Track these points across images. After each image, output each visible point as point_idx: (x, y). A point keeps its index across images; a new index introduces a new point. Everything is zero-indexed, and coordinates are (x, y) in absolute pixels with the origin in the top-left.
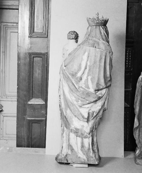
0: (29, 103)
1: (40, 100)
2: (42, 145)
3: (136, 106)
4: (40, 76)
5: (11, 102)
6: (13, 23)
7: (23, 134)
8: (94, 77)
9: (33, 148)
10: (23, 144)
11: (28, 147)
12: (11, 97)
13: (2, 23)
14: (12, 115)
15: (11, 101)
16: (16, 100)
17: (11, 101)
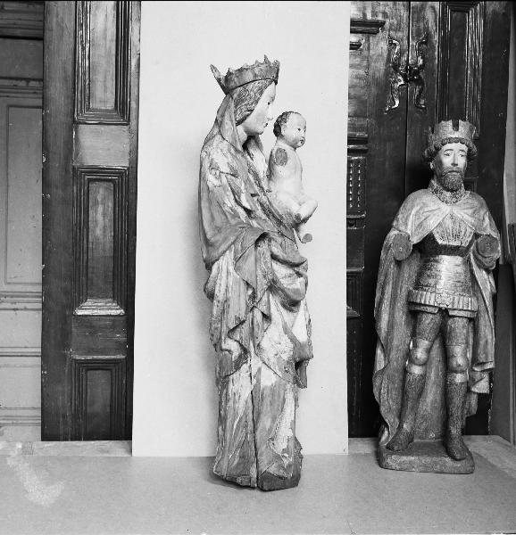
0: (80, 312)
1: (109, 302)
2: (118, 426)
3: (379, 312)
4: (110, 234)
5: (13, 312)
6: (17, 79)
7: (60, 404)
8: (273, 280)
9: (92, 442)
10: (62, 432)
11: (73, 439)
12: (12, 297)
13: (10, 109)
14: (18, 350)
15: (14, 310)
16: (40, 306)
17: (14, 310)
